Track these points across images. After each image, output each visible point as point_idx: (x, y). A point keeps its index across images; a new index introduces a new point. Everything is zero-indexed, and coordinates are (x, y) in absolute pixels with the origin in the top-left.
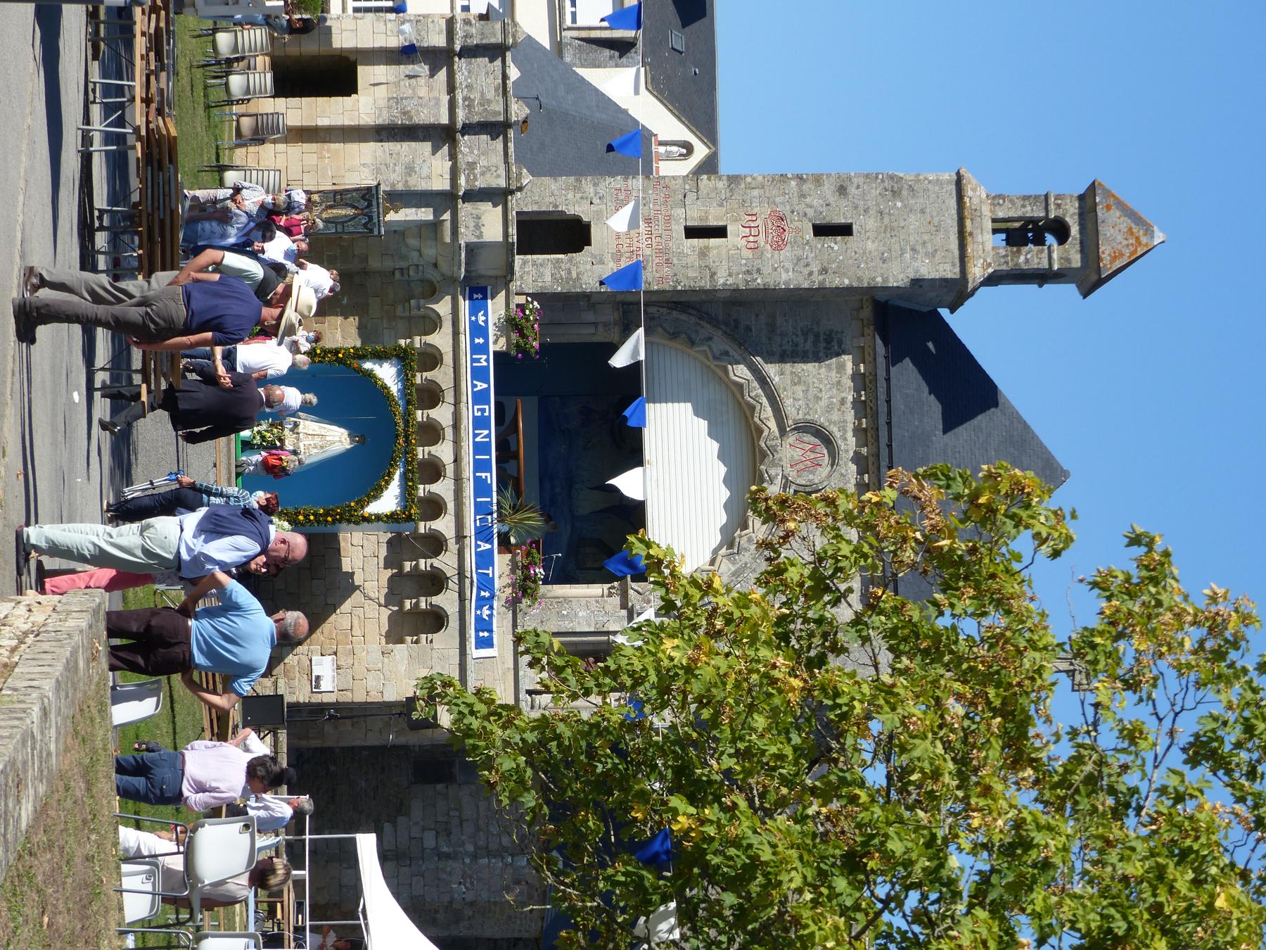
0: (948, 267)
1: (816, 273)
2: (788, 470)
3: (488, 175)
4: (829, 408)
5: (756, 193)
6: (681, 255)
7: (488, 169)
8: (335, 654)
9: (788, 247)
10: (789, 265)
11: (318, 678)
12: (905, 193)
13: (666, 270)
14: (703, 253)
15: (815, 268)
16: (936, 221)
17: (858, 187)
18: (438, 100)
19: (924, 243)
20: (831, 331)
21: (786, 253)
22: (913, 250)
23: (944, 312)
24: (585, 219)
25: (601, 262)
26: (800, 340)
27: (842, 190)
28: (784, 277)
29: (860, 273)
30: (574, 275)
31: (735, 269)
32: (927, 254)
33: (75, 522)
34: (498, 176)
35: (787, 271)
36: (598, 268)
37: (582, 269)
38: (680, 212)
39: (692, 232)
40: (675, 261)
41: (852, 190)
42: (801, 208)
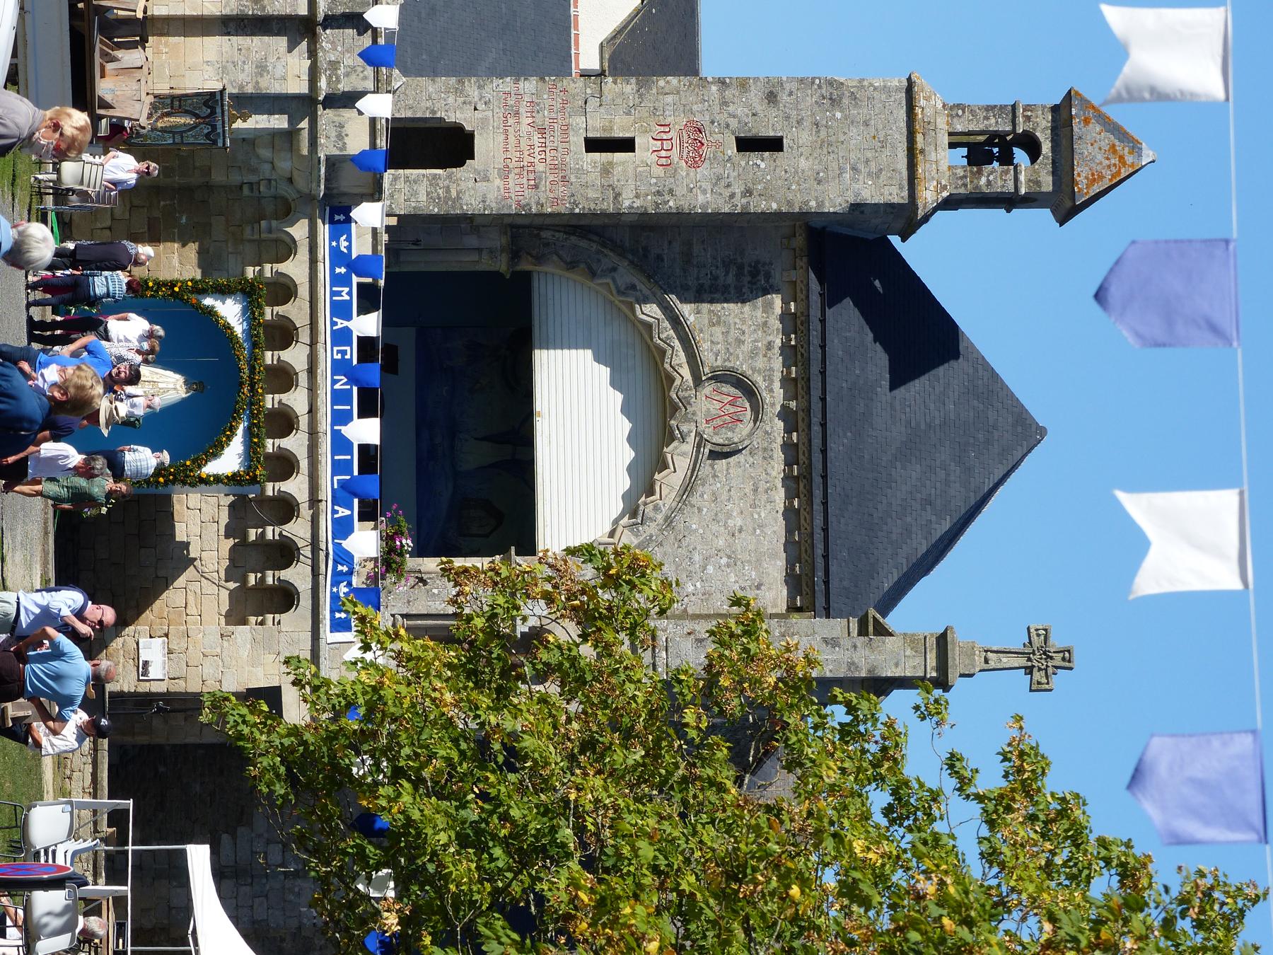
1: (738, 196)
2: (702, 425)
3: (354, 76)
5: (669, 99)
6: (580, 171)
8: (167, 635)
10: (707, 186)
11: (146, 663)
12: (846, 101)
13: (561, 190)
14: (606, 170)
15: (738, 189)
16: (881, 136)
17: (791, 94)
19: (867, 161)
20: (757, 262)
21: (704, 171)
22: (854, 169)
23: (895, 240)
24: (468, 128)
26: (720, 272)
27: (772, 98)
29: (790, 197)
30: (454, 194)
31: (643, 189)
32: (869, 174)
34: (365, 78)
35: (704, 192)
36: (482, 186)
37: (463, 186)
38: (579, 121)
39: (593, 145)
40: (573, 179)
41: (784, 97)
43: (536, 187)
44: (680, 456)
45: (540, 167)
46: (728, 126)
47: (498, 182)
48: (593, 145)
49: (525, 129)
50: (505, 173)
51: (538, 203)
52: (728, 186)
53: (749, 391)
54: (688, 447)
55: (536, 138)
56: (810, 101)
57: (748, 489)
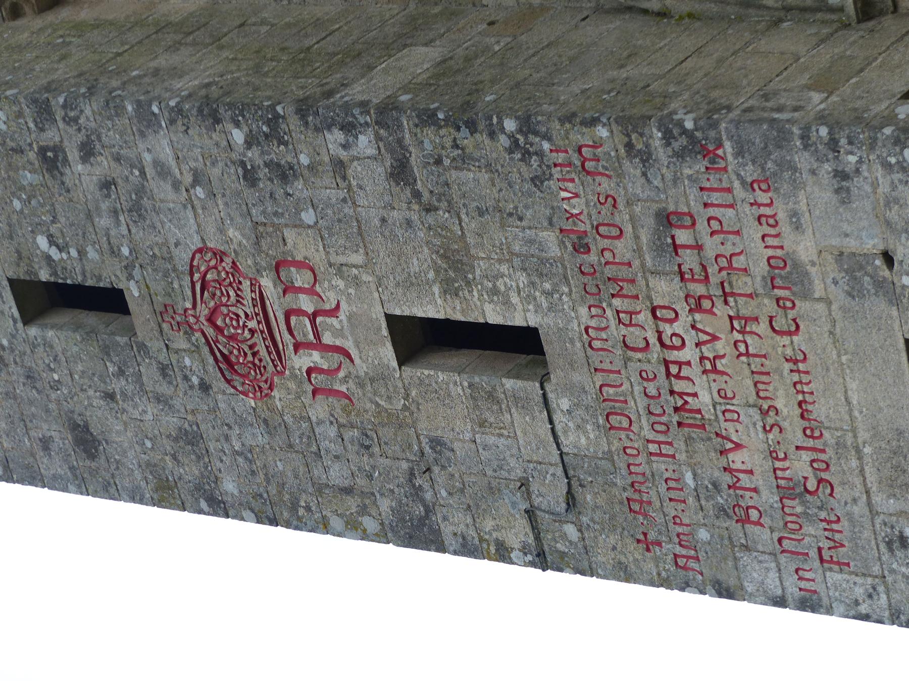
5: (337, 474)
6: (538, 267)
9: (182, 257)
10: (162, 190)
13: (577, 200)
15: (83, 175)
17: (46, 443)
25: (851, 265)
35: (163, 172)
39: (520, 345)
40: (550, 237)
43: (667, 220)
45: (665, 289)
46: (164, 370)
47: (804, 248)
49: (748, 431)
50: (785, 275)
51: (646, 158)
52: (107, 185)
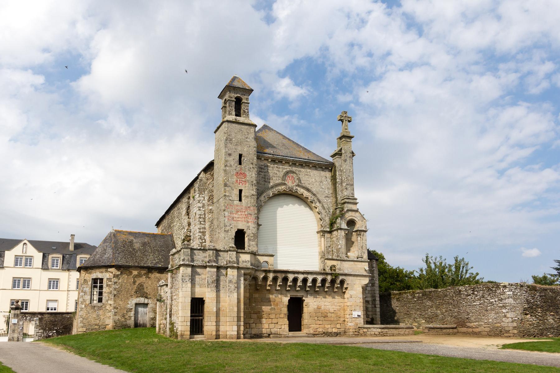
0: (252, 130)
2: (294, 185)
4: (279, 171)
5: (230, 179)
7: (230, 257)
10: (251, 173)
14: (247, 197)
15: (251, 166)
18: (209, 271)
21: (247, 173)
22: (247, 138)
25: (249, 227)
26: (261, 176)
27: (230, 155)
28: (254, 175)
31: (251, 188)
33: (71, 324)
36: (251, 228)
39: (240, 200)
41: (230, 152)
42: (234, 167)
44: (301, 191)
45: (246, 213)
47: (250, 224)
48: (240, 200)
49: (237, 216)
50: (248, 222)
53: (287, 173)
54: (299, 189)
55: (239, 213)
56: (230, 146)
57: (307, 176)
